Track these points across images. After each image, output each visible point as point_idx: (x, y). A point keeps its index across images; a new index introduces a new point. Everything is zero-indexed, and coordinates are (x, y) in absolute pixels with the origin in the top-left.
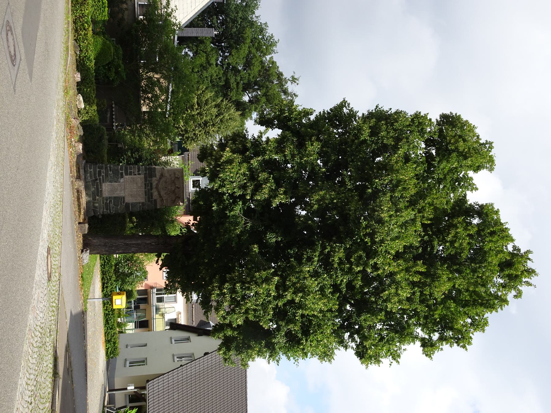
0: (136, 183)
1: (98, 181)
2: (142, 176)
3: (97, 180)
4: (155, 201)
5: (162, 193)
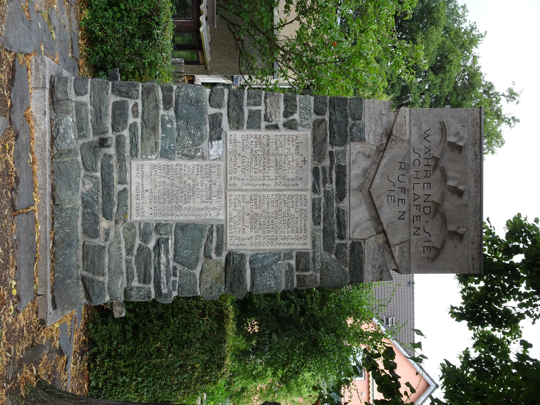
0: (278, 166)
1: (112, 151)
2: (305, 134)
3: (103, 143)
4: (357, 248)
5: (388, 213)
